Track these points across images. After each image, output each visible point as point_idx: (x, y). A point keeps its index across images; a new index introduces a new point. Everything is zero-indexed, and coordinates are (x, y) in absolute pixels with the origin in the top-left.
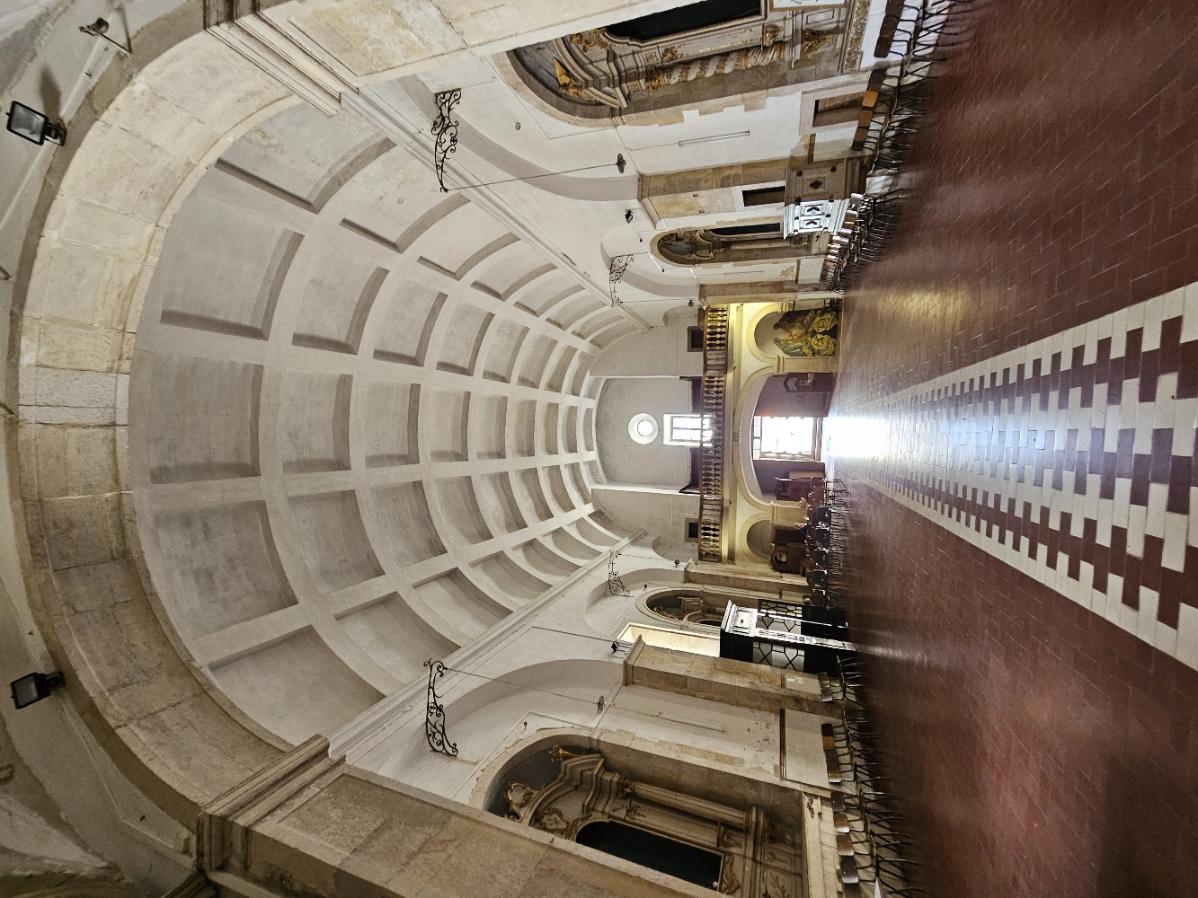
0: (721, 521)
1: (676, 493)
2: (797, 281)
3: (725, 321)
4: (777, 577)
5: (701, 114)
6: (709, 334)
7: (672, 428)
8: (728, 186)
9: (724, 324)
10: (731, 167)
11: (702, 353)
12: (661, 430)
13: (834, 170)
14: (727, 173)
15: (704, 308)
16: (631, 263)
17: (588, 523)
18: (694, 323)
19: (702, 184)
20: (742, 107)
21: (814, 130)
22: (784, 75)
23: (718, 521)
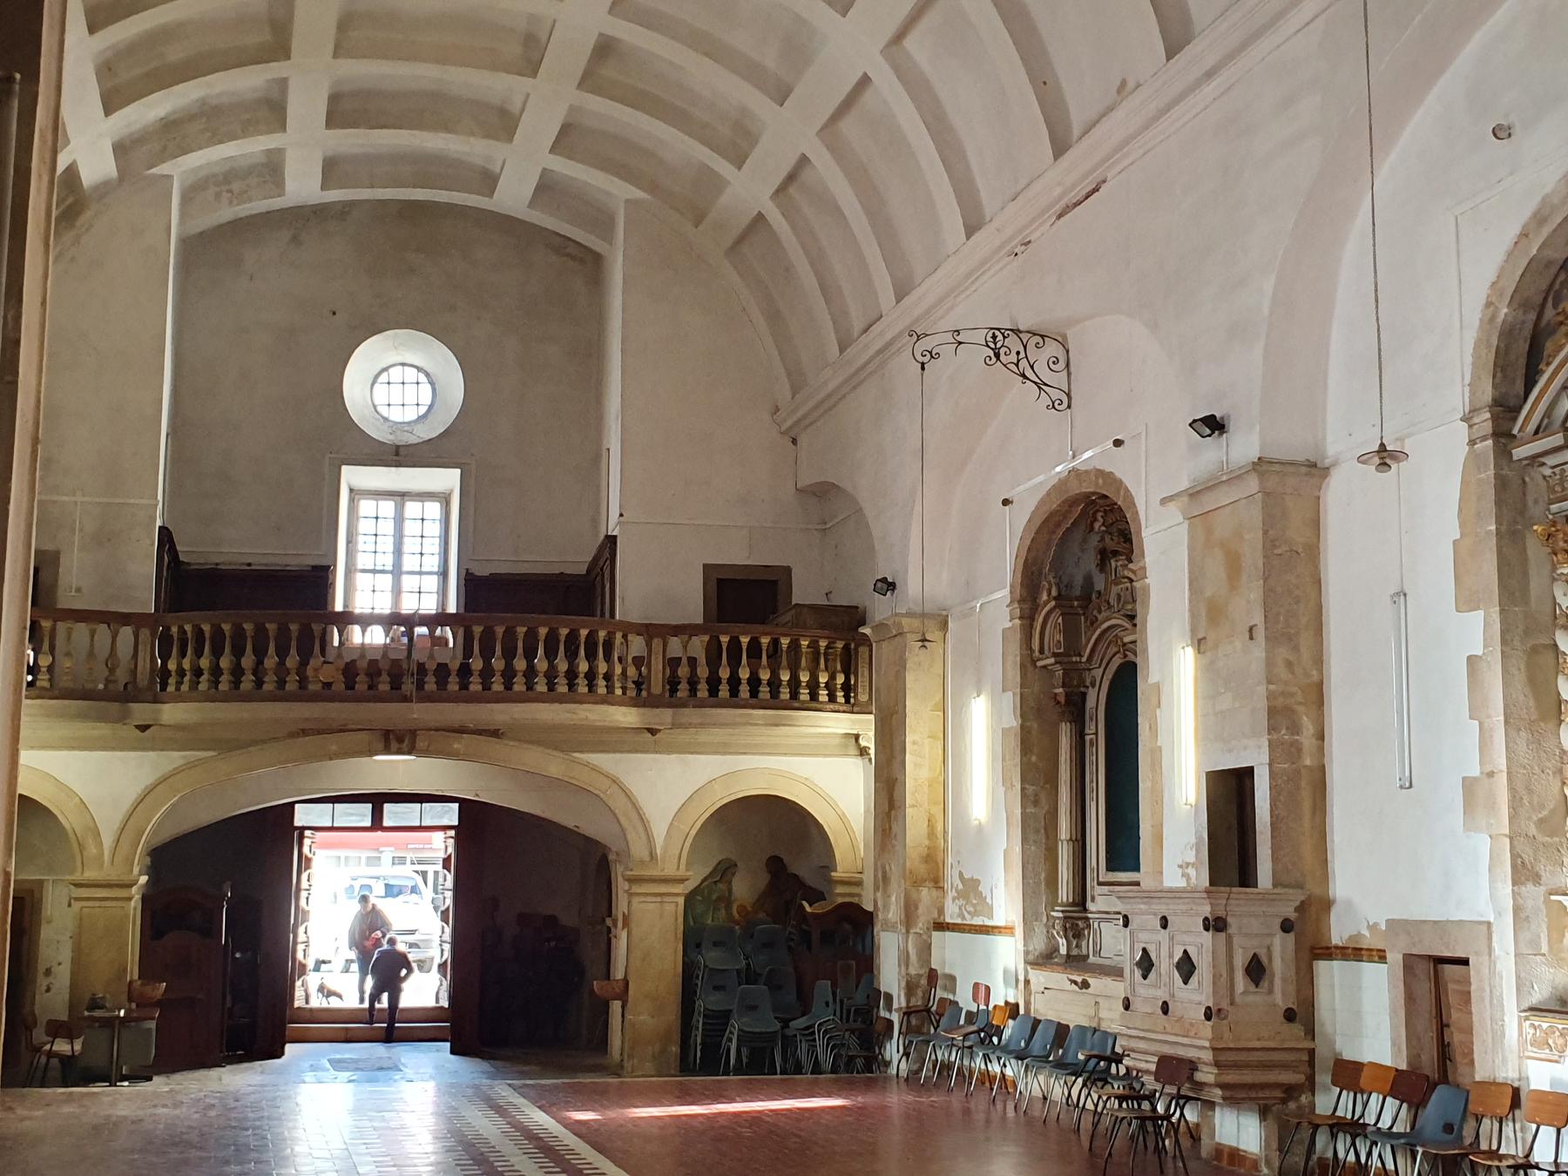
2: (941, 926)
3: (814, 696)
5: (1471, 660)
7: (401, 496)
8: (1272, 729)
9: (804, 695)
10: (1321, 736)
11: (700, 620)
12: (398, 455)
13: (1290, 1015)
14: (1308, 727)
15: (866, 630)
16: (1046, 401)
18: (804, 592)
19: (1283, 653)
20: (1475, 771)
21: (1395, 957)
22: (1536, 879)
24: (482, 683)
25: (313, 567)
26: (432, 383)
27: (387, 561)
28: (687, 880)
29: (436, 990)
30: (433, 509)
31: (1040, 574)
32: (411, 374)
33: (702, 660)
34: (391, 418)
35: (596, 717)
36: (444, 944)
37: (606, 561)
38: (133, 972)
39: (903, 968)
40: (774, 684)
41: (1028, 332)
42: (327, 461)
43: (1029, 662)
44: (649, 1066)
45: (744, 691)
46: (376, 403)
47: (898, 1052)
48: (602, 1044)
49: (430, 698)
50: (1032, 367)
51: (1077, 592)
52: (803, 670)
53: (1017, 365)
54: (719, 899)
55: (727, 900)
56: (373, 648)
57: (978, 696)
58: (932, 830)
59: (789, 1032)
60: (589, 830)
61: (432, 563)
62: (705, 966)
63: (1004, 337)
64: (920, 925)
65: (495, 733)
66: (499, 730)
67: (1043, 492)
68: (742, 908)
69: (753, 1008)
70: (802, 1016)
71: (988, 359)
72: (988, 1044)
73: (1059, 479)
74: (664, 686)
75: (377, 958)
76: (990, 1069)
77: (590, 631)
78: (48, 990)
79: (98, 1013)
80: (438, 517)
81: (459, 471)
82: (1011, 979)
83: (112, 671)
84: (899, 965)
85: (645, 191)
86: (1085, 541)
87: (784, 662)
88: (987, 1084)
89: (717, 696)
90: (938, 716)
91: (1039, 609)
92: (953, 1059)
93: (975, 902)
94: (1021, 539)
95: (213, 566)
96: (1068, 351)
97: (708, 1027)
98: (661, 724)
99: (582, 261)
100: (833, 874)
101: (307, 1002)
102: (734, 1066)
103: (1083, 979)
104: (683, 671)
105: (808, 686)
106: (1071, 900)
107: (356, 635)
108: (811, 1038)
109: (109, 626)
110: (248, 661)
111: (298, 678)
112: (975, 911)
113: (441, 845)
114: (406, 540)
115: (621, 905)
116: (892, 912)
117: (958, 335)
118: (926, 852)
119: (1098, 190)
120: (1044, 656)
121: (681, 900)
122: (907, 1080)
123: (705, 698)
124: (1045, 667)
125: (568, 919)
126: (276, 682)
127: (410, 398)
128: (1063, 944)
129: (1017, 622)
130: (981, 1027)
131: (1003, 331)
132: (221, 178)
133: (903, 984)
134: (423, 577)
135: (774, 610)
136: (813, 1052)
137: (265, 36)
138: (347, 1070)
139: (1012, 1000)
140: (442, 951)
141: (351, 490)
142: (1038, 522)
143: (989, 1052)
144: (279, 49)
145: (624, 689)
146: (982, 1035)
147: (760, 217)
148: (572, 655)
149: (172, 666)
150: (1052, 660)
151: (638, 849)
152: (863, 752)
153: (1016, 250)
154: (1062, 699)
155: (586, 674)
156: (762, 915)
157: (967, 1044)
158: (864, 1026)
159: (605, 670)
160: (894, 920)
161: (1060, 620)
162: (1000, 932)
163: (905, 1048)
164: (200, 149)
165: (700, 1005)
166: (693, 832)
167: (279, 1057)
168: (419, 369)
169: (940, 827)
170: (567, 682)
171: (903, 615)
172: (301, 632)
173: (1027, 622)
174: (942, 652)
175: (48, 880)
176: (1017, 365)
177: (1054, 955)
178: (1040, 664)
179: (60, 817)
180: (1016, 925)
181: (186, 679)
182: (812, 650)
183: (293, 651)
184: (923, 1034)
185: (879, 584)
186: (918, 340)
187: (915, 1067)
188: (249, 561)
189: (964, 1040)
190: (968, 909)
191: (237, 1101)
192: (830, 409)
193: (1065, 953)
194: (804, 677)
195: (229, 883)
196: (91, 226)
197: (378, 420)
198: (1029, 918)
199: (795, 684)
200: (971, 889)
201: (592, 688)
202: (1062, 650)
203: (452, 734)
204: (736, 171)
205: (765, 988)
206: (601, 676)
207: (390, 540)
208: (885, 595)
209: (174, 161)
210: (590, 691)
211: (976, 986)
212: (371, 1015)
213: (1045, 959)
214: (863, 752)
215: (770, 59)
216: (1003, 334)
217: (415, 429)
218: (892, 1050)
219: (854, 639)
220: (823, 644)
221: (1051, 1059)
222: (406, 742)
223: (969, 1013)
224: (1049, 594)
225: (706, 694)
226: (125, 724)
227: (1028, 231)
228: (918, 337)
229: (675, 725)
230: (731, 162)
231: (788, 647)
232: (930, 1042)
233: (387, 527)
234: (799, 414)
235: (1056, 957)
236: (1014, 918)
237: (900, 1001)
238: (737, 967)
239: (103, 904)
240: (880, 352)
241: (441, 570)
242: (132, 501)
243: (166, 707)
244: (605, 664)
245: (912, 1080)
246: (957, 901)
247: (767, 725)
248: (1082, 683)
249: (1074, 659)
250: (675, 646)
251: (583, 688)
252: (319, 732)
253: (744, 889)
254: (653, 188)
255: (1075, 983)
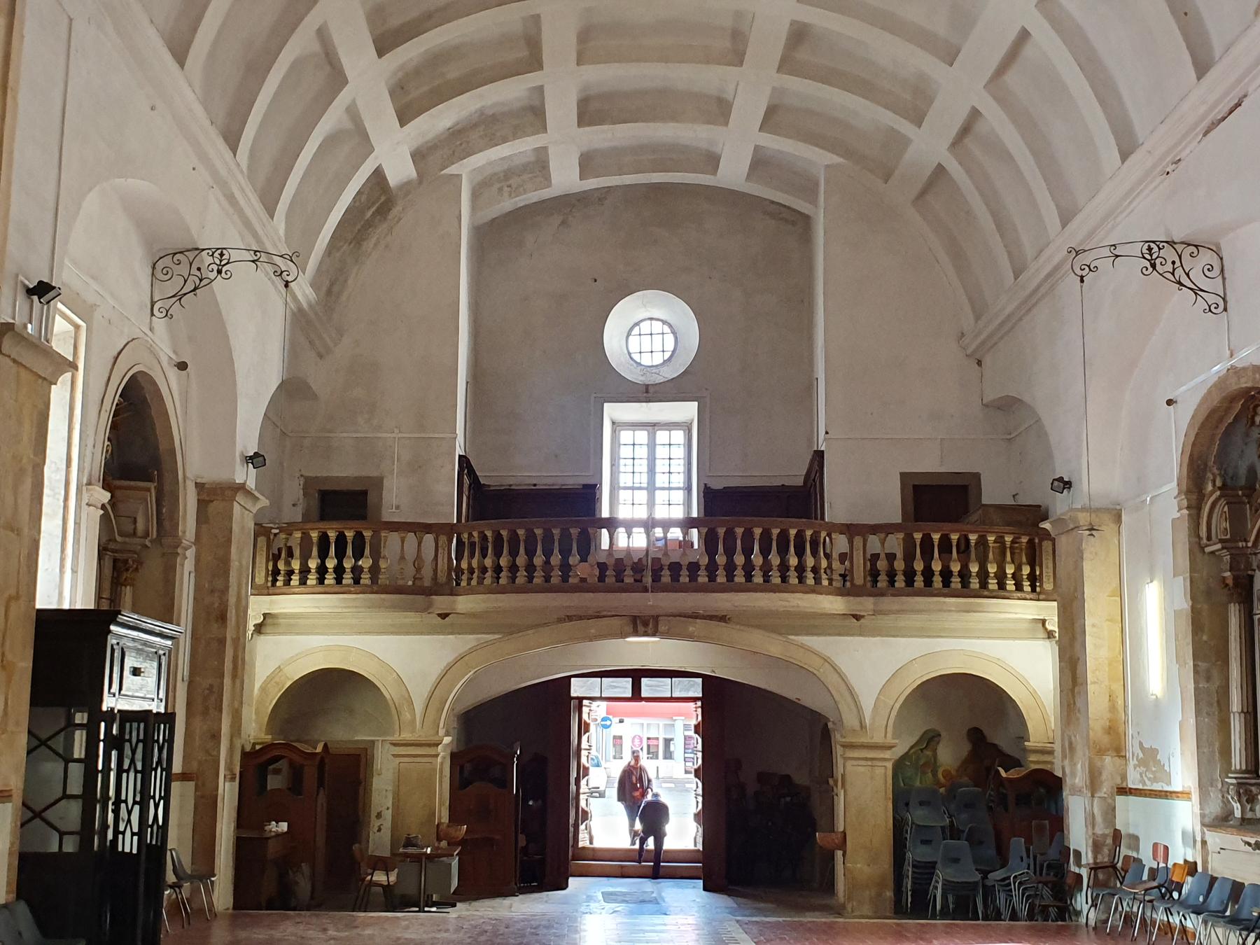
0: (385, 590)
1: (459, 451)
2: (1123, 791)
3: (1002, 586)
4: (229, 768)
6: (800, 536)
7: (652, 427)
9: (993, 584)
12: (648, 393)
15: (1046, 525)
16: (1201, 304)
17: (356, 168)
18: (993, 493)
23: (383, 579)
24: (708, 576)
25: (583, 485)
26: (674, 333)
27: (644, 479)
28: (893, 747)
29: (694, 835)
30: (678, 436)
31: (1206, 465)
32: (658, 326)
33: (900, 555)
34: (642, 363)
35: (805, 604)
36: (698, 797)
37: (816, 473)
38: (444, 816)
39: (1090, 828)
40: (964, 575)
41: (1182, 243)
42: (592, 399)
43: (1197, 548)
44: (866, 910)
45: (937, 581)
46: (631, 351)
47: (1087, 903)
48: (829, 886)
49: (666, 589)
50: (1188, 275)
51: (1242, 482)
52: (991, 563)
53: (1173, 274)
54: (925, 765)
55: (933, 765)
56: (638, 550)
57: (1151, 581)
58: (1114, 705)
59: (989, 883)
60: (808, 701)
61: (679, 480)
62: (913, 823)
63: (1160, 249)
64: (1105, 790)
65: (723, 619)
66: (726, 616)
67: (1203, 391)
68: (947, 774)
69: (956, 861)
70: (1001, 868)
71: (1144, 269)
72: (1168, 899)
73: (1219, 378)
74: (865, 579)
75: (644, 807)
76: (1171, 920)
77: (798, 531)
78: (379, 830)
79: (411, 850)
80: (682, 443)
81: (696, 403)
82: (1189, 839)
83: (418, 570)
84: (1086, 826)
85: (842, 156)
86: (1247, 435)
87: (973, 556)
88: (1170, 935)
89: (913, 586)
90: (1115, 601)
91: (1206, 499)
92: (1135, 909)
93: (1154, 769)
94: (1185, 436)
95: (508, 487)
96: (1221, 259)
97: (916, 875)
98: (865, 611)
99: (794, 223)
100: (1026, 743)
101: (591, 842)
102: (940, 911)
103: (1256, 841)
104: (882, 565)
105: (996, 576)
106: (1244, 767)
107: (622, 541)
108: (1008, 888)
109: (415, 534)
110: (521, 560)
111: (560, 573)
112: (1155, 777)
113: (692, 714)
114: (658, 462)
115: (839, 770)
116: (1075, 776)
117: (1114, 249)
118: (1108, 724)
119: (1240, 105)
120: (1211, 542)
121: (889, 765)
122: (1095, 928)
123: (902, 588)
124: (1213, 553)
125: (800, 778)
126: (544, 577)
127: (657, 346)
128: (1237, 809)
129: (1185, 512)
130: (1162, 883)
131: (1158, 243)
132: (502, 175)
133: (1090, 842)
134: (671, 492)
135: (966, 511)
136: (1010, 901)
137: (523, 53)
138: (615, 901)
139: (1190, 859)
140: (697, 802)
141: (613, 423)
142: (1201, 418)
143: (1169, 906)
144: (534, 62)
145: (831, 580)
146: (1163, 890)
147: (940, 170)
148: (783, 551)
149: (464, 565)
150: (1219, 546)
151: (850, 720)
152: (1050, 635)
153: (1168, 170)
154: (1230, 582)
155: (796, 567)
156: (965, 779)
157: (1147, 898)
158: (1055, 879)
159: (812, 565)
160: (1080, 785)
161: (1226, 509)
162: (1178, 797)
163: (1092, 901)
164: (481, 151)
165: (909, 855)
166: (898, 706)
167: (564, 889)
168: (664, 322)
169: (1120, 702)
170: (779, 574)
171: (1077, 510)
172: (562, 535)
173: (1194, 512)
174: (1117, 542)
175: (378, 740)
176: (1173, 274)
177: (1230, 818)
178: (1208, 550)
179: (383, 689)
180: (1192, 790)
181: (475, 576)
182: (998, 545)
183: (556, 551)
184: (1110, 888)
185: (1056, 483)
186: (1076, 256)
187: (1104, 917)
188: (535, 483)
189: (1144, 895)
190: (1148, 776)
191: (507, 927)
192: (1009, 331)
193: (1240, 816)
194: (992, 569)
195: (518, 743)
196: (400, 219)
197: (632, 365)
198: (1204, 785)
199: (983, 576)
200: (1150, 758)
201: (801, 579)
202: (1228, 537)
203: (690, 620)
204: (917, 129)
205: (966, 842)
206: (809, 569)
207: (645, 462)
208: (1062, 493)
209: (461, 162)
210: (800, 582)
211: (1155, 846)
212: (640, 856)
213: (1222, 821)
214: (1050, 635)
215: (940, 26)
216: (1158, 246)
217: (662, 371)
218: (1082, 902)
219: (1038, 534)
220: (1008, 539)
221: (1228, 913)
222: (651, 626)
223: (1151, 869)
224: (1214, 485)
225: (903, 584)
226: (429, 613)
227: (1180, 148)
228: (1077, 252)
229: (876, 613)
230: (912, 121)
231: (975, 545)
232: (1114, 895)
233: (642, 452)
234: (982, 337)
235: (1231, 820)
236: (1190, 784)
237: (1088, 858)
238: (942, 825)
239: (418, 759)
240: (1049, 275)
241: (686, 486)
242: (436, 436)
243: (460, 598)
244: (812, 559)
245: (1099, 928)
246: (1138, 768)
247: (959, 611)
248: (1249, 566)
249: (1240, 544)
250: (874, 544)
251: (794, 580)
252: (580, 618)
253: (949, 755)
254: (847, 153)
255: (1249, 844)
